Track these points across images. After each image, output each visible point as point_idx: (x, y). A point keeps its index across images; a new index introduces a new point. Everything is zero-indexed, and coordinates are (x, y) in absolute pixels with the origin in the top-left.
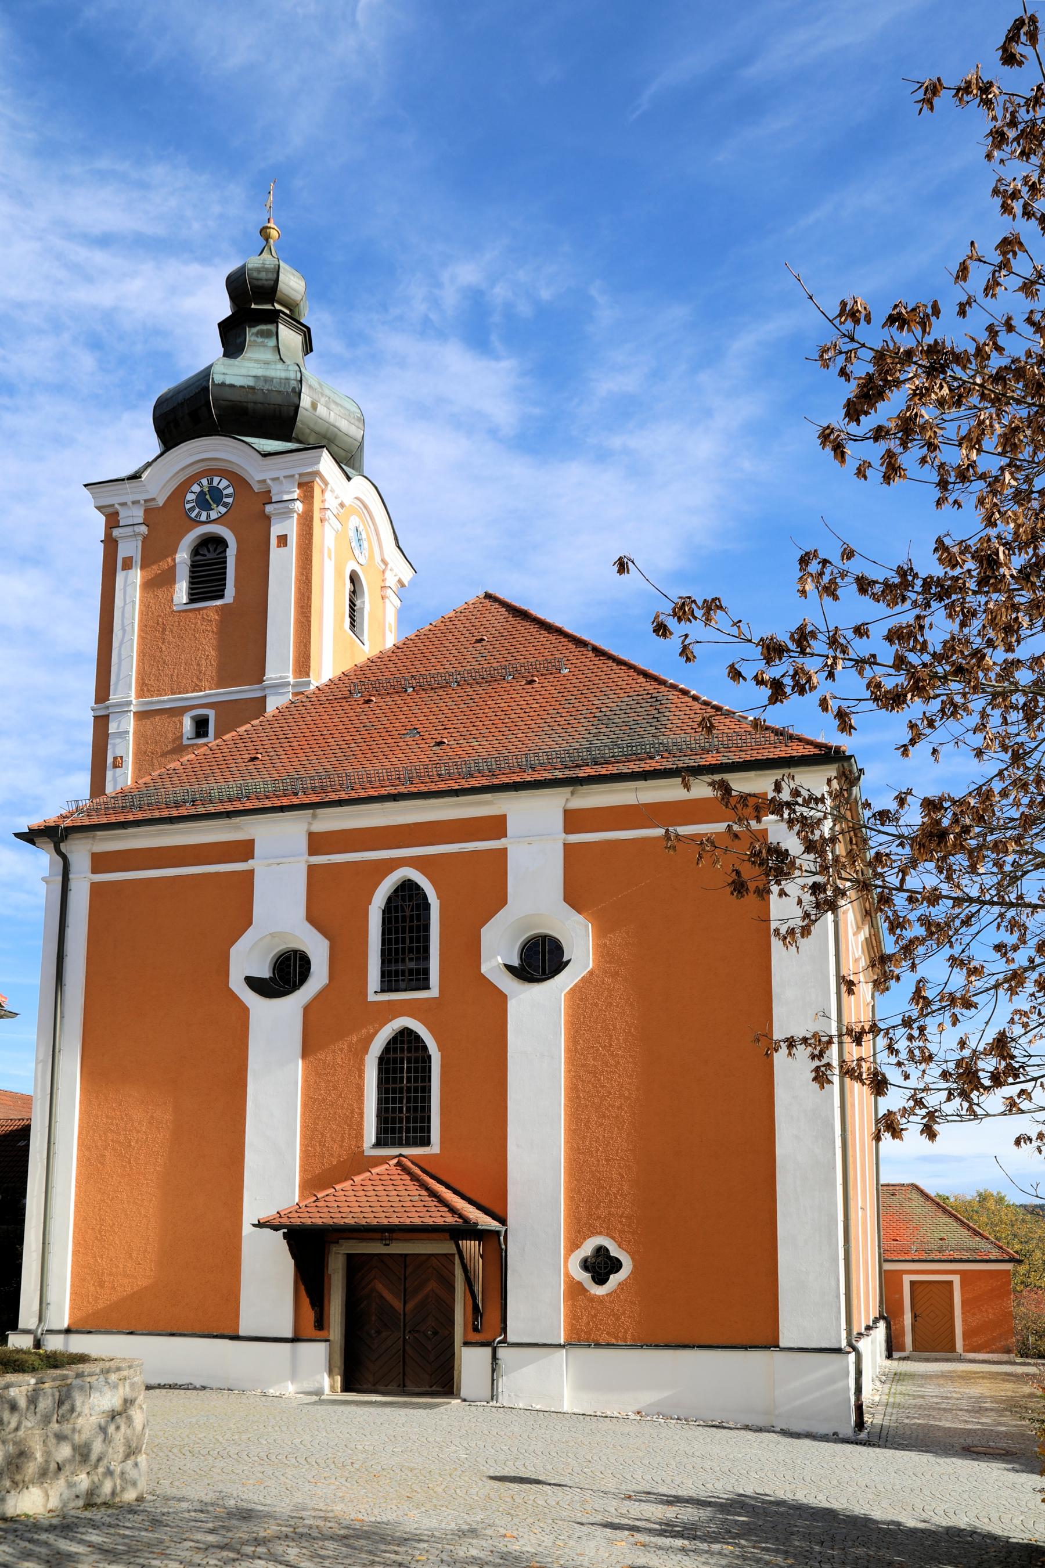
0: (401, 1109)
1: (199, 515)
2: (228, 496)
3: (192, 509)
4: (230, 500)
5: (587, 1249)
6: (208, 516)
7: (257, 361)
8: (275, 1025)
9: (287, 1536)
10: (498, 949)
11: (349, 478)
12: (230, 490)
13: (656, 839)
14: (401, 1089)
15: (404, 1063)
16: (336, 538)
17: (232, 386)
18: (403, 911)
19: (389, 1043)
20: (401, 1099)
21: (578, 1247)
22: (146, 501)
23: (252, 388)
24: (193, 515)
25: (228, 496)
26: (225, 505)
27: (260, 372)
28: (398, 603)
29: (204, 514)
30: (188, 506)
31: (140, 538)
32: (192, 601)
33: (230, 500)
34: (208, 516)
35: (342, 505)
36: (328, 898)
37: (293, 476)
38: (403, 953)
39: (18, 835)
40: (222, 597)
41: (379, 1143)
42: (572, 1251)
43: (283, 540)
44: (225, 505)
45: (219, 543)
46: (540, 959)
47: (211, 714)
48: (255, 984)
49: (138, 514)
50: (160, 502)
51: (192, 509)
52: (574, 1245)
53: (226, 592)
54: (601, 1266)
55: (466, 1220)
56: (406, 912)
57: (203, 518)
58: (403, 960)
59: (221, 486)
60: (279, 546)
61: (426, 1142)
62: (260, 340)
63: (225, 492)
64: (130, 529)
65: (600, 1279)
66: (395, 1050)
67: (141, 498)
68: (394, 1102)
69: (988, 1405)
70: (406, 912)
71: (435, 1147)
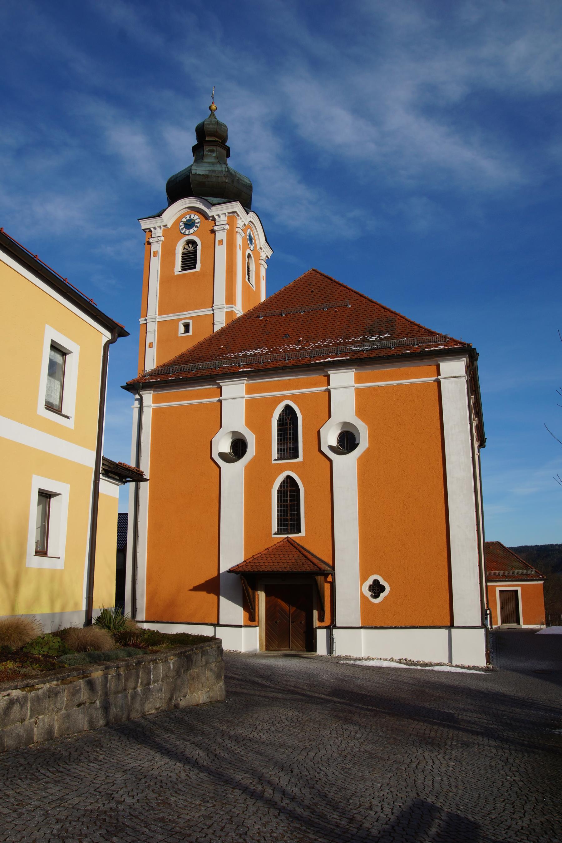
0: (287, 514)
1: (185, 231)
2: (198, 223)
3: (182, 229)
4: (198, 225)
5: (370, 582)
6: (189, 232)
7: (209, 163)
8: (233, 475)
9: (230, 738)
10: (331, 437)
11: (248, 213)
12: (198, 220)
13: (211, 404)
14: (287, 505)
15: (289, 492)
16: (242, 240)
17: (199, 175)
18: (286, 420)
19: (281, 483)
20: (287, 510)
21: (367, 580)
22: (164, 226)
23: (206, 176)
24: (183, 232)
25: (198, 223)
26: (197, 227)
27: (210, 168)
28: (266, 266)
29: (187, 231)
30: (181, 228)
31: (161, 242)
32: (183, 270)
33: (198, 225)
34: (189, 232)
35: (245, 225)
36: (255, 412)
37: (225, 214)
38: (287, 440)
39: (123, 387)
40: (195, 268)
41: (279, 532)
42: (364, 582)
43: (221, 242)
44: (197, 227)
45: (193, 243)
46: (151, 345)
47: (191, 322)
48: (222, 456)
49: (159, 232)
50: (169, 226)
51: (182, 229)
52: (364, 579)
53: (197, 266)
54: (376, 589)
55: (320, 569)
56: (288, 420)
57: (187, 233)
58: (287, 443)
59: (195, 218)
60: (219, 245)
61: (299, 531)
62: (209, 153)
63: (196, 221)
64: (157, 238)
65: (376, 596)
66: (284, 487)
67: (162, 225)
68: (284, 512)
69: (238, 777)
70: (288, 420)
71: (303, 533)
